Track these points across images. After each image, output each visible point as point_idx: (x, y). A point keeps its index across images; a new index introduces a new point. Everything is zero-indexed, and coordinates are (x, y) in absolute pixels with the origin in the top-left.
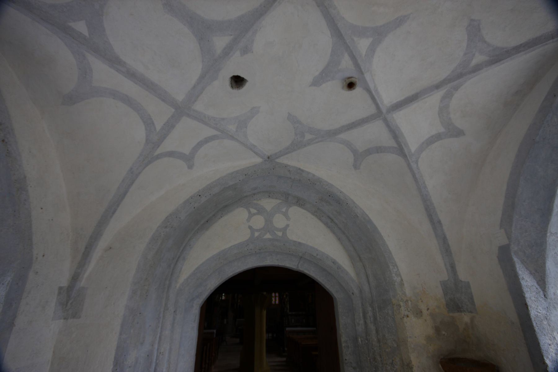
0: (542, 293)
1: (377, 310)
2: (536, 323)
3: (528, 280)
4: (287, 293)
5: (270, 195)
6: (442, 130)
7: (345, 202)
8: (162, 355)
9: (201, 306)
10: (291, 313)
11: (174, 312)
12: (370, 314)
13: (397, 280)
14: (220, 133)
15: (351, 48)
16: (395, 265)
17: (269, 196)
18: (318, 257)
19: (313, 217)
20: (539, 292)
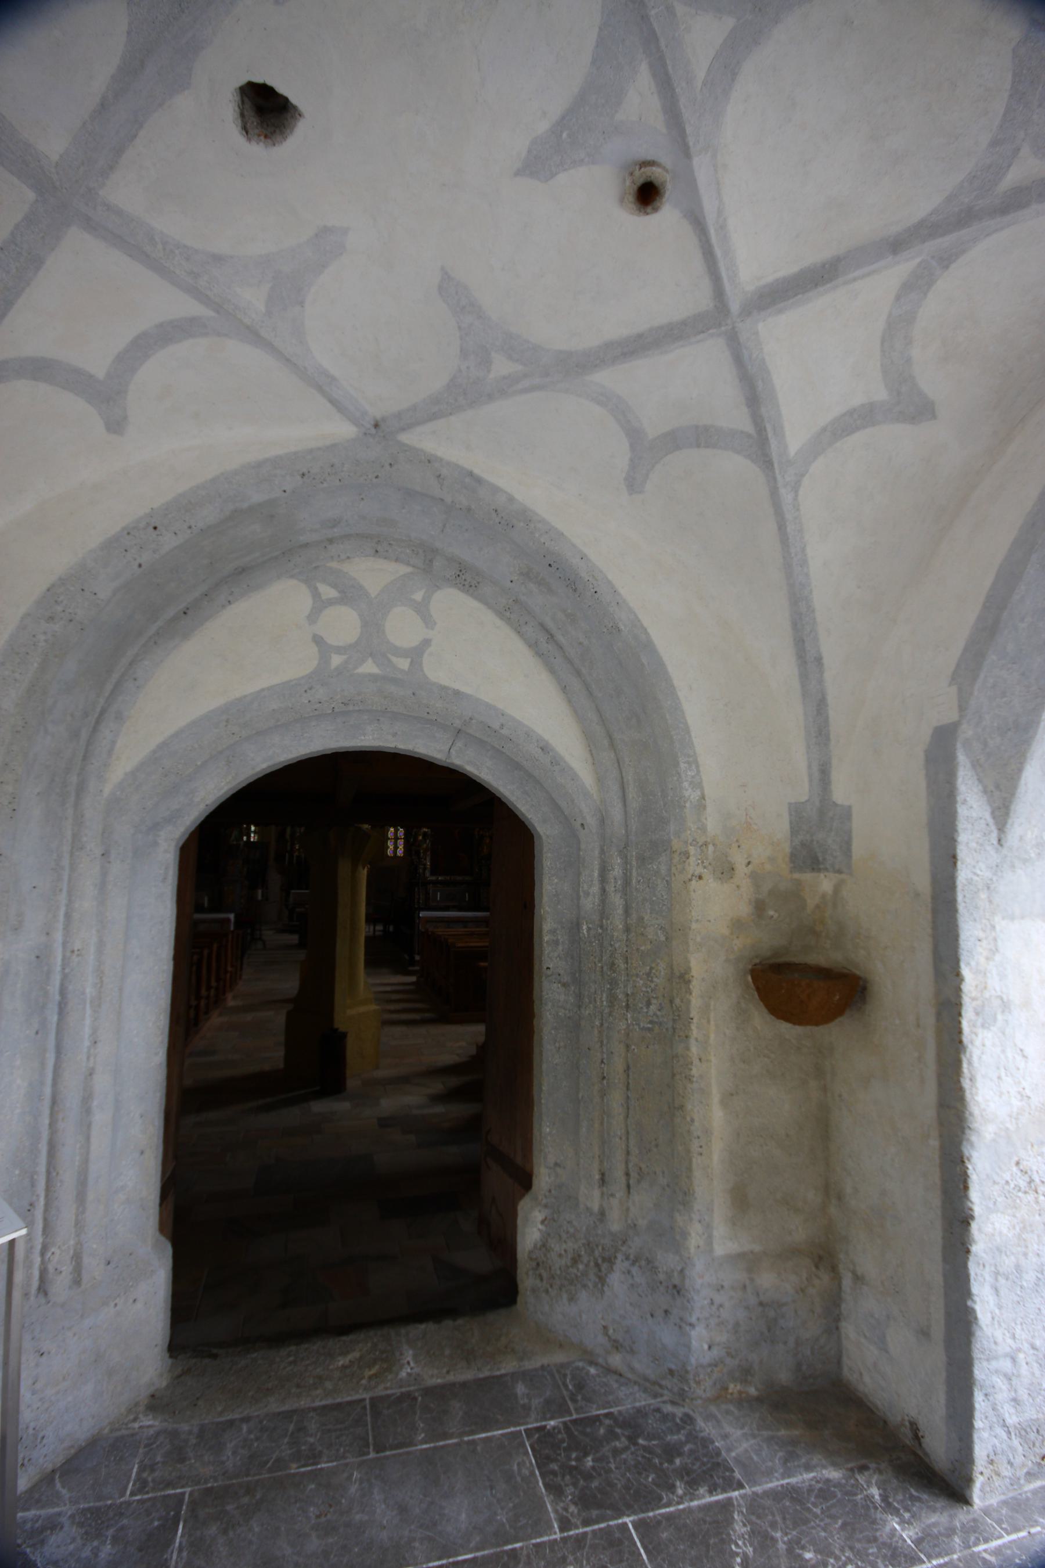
0: (994, 835)
1: (634, 863)
2: (965, 896)
3: (975, 806)
4: (425, 830)
5: (379, 548)
6: (881, 394)
7: (591, 586)
8: (78, 955)
9: (181, 843)
10: (434, 878)
11: (103, 855)
12: (617, 872)
13: (692, 797)
14: (212, 314)
15: (663, 43)
16: (694, 762)
17: (377, 551)
18: (504, 732)
19: (499, 622)
20: (991, 831)
